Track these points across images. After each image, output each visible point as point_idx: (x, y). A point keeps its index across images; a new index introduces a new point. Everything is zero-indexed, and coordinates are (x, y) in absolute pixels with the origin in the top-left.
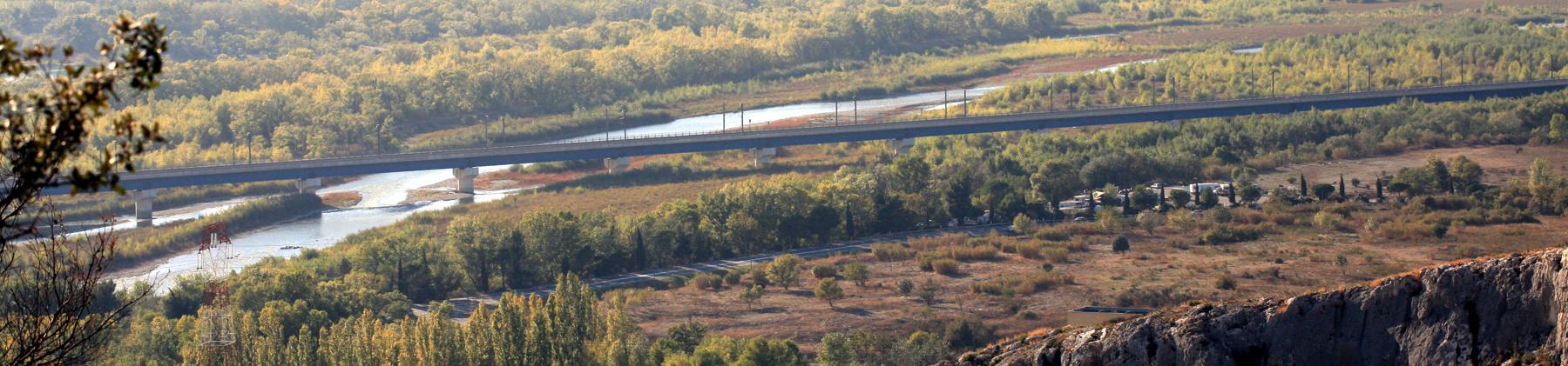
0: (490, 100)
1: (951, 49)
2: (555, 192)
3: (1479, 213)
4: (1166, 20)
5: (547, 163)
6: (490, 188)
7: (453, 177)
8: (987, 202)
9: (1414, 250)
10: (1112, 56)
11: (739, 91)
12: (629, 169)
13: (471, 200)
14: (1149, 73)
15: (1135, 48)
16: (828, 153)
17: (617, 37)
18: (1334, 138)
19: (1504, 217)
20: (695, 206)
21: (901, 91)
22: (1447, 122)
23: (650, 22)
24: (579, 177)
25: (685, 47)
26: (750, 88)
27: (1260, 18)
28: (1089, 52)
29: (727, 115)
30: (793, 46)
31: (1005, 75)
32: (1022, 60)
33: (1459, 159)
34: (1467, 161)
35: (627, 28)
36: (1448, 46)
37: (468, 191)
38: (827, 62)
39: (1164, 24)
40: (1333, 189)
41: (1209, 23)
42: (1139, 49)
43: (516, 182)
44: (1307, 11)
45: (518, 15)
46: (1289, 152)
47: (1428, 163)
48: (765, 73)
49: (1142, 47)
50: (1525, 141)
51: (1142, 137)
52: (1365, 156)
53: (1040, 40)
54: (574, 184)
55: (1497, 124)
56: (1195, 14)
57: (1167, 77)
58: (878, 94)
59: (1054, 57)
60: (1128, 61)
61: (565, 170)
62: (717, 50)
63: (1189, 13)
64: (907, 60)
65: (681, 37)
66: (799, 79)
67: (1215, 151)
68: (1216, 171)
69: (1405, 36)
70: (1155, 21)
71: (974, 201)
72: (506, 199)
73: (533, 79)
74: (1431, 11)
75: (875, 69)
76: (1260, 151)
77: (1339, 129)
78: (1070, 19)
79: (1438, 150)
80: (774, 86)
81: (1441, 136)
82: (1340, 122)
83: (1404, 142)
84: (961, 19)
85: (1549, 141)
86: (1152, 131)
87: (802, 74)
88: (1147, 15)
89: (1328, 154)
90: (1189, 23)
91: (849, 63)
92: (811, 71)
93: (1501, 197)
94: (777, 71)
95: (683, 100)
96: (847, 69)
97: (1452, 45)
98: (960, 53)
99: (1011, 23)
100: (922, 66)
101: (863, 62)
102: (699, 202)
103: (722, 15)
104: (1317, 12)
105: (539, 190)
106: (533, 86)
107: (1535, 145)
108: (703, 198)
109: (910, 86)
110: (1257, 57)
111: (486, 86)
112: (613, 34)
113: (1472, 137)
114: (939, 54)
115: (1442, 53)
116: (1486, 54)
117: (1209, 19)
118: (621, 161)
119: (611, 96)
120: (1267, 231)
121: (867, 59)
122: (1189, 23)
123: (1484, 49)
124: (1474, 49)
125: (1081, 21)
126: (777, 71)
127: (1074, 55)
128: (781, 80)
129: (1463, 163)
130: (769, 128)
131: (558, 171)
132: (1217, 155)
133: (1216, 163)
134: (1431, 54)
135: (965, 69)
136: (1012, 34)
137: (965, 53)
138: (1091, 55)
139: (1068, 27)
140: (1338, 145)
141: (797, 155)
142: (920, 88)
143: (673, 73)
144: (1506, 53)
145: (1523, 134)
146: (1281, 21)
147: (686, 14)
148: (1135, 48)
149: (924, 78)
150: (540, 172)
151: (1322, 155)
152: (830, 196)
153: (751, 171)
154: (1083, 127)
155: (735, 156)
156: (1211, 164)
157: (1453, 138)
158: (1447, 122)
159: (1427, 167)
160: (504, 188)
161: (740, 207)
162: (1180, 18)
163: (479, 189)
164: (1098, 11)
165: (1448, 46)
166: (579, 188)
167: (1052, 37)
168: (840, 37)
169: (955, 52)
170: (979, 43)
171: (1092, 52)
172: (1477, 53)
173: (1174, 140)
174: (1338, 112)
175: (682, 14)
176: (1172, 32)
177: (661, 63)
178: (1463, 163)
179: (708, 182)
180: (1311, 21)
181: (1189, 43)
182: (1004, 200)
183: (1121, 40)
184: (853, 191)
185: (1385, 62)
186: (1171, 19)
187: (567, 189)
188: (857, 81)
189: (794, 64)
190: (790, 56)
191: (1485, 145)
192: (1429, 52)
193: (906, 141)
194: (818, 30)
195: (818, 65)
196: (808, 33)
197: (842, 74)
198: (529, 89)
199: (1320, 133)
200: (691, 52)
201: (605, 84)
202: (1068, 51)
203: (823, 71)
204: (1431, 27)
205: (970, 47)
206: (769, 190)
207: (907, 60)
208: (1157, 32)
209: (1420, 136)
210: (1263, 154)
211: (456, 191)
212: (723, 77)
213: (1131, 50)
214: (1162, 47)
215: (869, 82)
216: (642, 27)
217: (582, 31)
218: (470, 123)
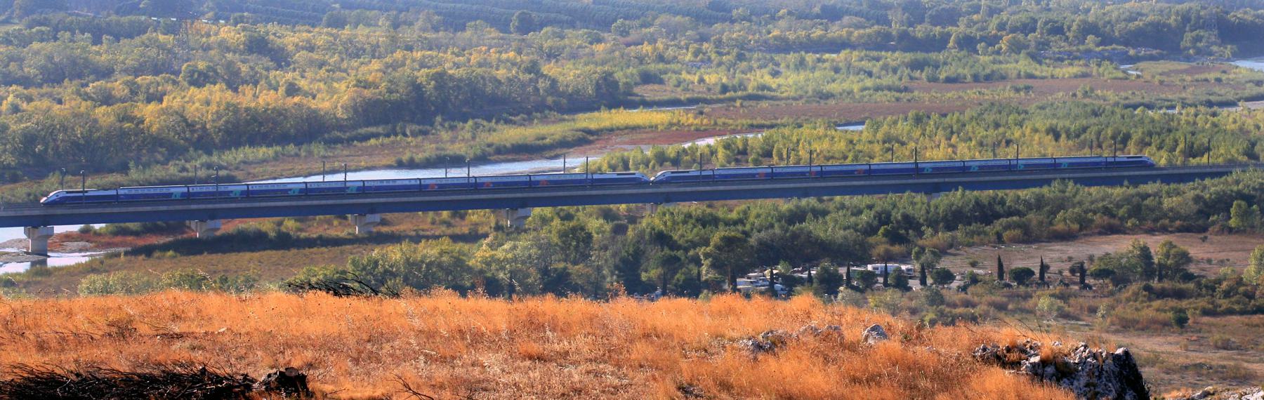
0: (34, 155)
1: (519, 117)
2: (143, 257)
3: (1209, 303)
4: (739, 93)
5: (122, 225)
6: (64, 251)
7: (25, 237)
8: (659, 277)
9: (1160, 339)
10: (697, 130)
11: (303, 154)
12: (218, 233)
13: (44, 262)
14: (752, 148)
15: (720, 121)
16: (433, 223)
17: (147, 92)
18: (1004, 221)
19: (1236, 307)
20: (344, 272)
21: (482, 159)
22: (1119, 206)
23: (180, 79)
24: (162, 242)
25: (239, 104)
26: (316, 151)
27: (841, 94)
28: (671, 124)
29: (348, 174)
30: (352, 107)
31: (588, 147)
32: (601, 130)
33: (1165, 245)
34: (1175, 247)
35: (158, 84)
36: (1069, 129)
37: (40, 253)
38: (390, 126)
39: (741, 98)
40: (1033, 273)
41: (787, 98)
42: (724, 124)
43: (92, 245)
44: (890, 89)
45: (30, 66)
46: (959, 234)
47: (1131, 248)
48: (326, 136)
49: (727, 121)
50: (1204, 229)
51: (787, 214)
52: (1037, 240)
53: (613, 111)
54: (165, 248)
55: (1171, 210)
56: (769, 89)
57: (774, 152)
58: (457, 161)
59: (634, 129)
60: (725, 135)
61: (144, 232)
62: (274, 109)
63: (763, 87)
64: (477, 126)
65: (217, 93)
66: (364, 144)
67: (882, 230)
68: (887, 251)
69: (1020, 118)
70: (728, 95)
71: (644, 277)
72: (91, 262)
73: (82, 134)
74: (1022, 93)
75: (445, 135)
76: (929, 231)
77: (1002, 211)
78: (637, 90)
79: (1115, 236)
80: (339, 150)
81: (1116, 222)
82: (1002, 202)
83: (1076, 226)
84: (524, 85)
85: (1231, 231)
86: (798, 207)
87: (366, 138)
88: (718, 88)
89: (999, 237)
90: (765, 98)
91: (416, 127)
92: (376, 136)
93: (1225, 285)
94: (339, 134)
95: (245, 162)
96: (414, 134)
97: (1073, 128)
98: (530, 120)
99: (577, 92)
100: (495, 134)
101: (428, 128)
102: (349, 267)
103: (257, 73)
104: (899, 90)
105: (126, 253)
106: (82, 141)
107: (1217, 233)
108: (354, 263)
109: (490, 155)
110: (865, 134)
111: (29, 139)
112: (143, 89)
113: (1149, 224)
114: (507, 122)
115: (1063, 136)
116: (1113, 138)
117: (785, 95)
118: (210, 224)
119: (163, 155)
120: (985, 316)
121: (432, 125)
122: (765, 98)
123: (1109, 132)
124: (1099, 133)
125: (648, 92)
126: (339, 134)
127: (656, 126)
128: (345, 145)
129: (1170, 248)
130: (861, 180)
131: (136, 234)
132: (884, 235)
133: (884, 243)
134: (1050, 137)
135: (543, 138)
136: (576, 104)
137: (536, 121)
138: (674, 128)
139: (637, 99)
140: (1007, 227)
141: (399, 224)
142: (501, 157)
143: (227, 132)
144: (1135, 137)
145: (1201, 222)
146: (865, 100)
147: (219, 71)
148: (720, 121)
149: (505, 146)
150: (116, 234)
151: (993, 238)
152: (488, 264)
153: (354, 241)
154: (707, 202)
155: (330, 223)
156: (879, 243)
157: (1129, 224)
158: (1119, 206)
159: (1130, 252)
160: (80, 251)
161: (394, 275)
162: (755, 92)
163: (52, 251)
164: (661, 82)
165: (1069, 129)
166: (171, 253)
167: (625, 108)
168: (402, 100)
169: (524, 120)
170: (547, 112)
171: (675, 124)
172: (1102, 137)
173: (828, 218)
174: (1000, 193)
175: (215, 71)
176: (778, 105)
177: (213, 121)
178: (1170, 248)
179: (312, 250)
180: (898, 100)
181: (776, 118)
182: (678, 276)
183: (701, 113)
184: (515, 260)
185: (1003, 143)
186: (744, 93)
187: (157, 254)
188: (429, 149)
189: (354, 127)
190: (349, 119)
191: (1163, 233)
192: (1048, 134)
193: (521, 212)
194: (377, 91)
195: (380, 129)
196: (368, 93)
197: (410, 139)
198: (75, 144)
199: (986, 214)
200: (247, 109)
201: (157, 142)
202: (647, 123)
203: (388, 136)
204: (1042, 108)
205: (538, 115)
206: (425, 256)
207: (477, 126)
208: (735, 107)
209: (1092, 221)
210: (932, 236)
211: (27, 253)
212: (284, 139)
213: (716, 124)
214: (749, 122)
215: (443, 149)
216: (175, 83)
217: (109, 85)
218: (15, 179)
